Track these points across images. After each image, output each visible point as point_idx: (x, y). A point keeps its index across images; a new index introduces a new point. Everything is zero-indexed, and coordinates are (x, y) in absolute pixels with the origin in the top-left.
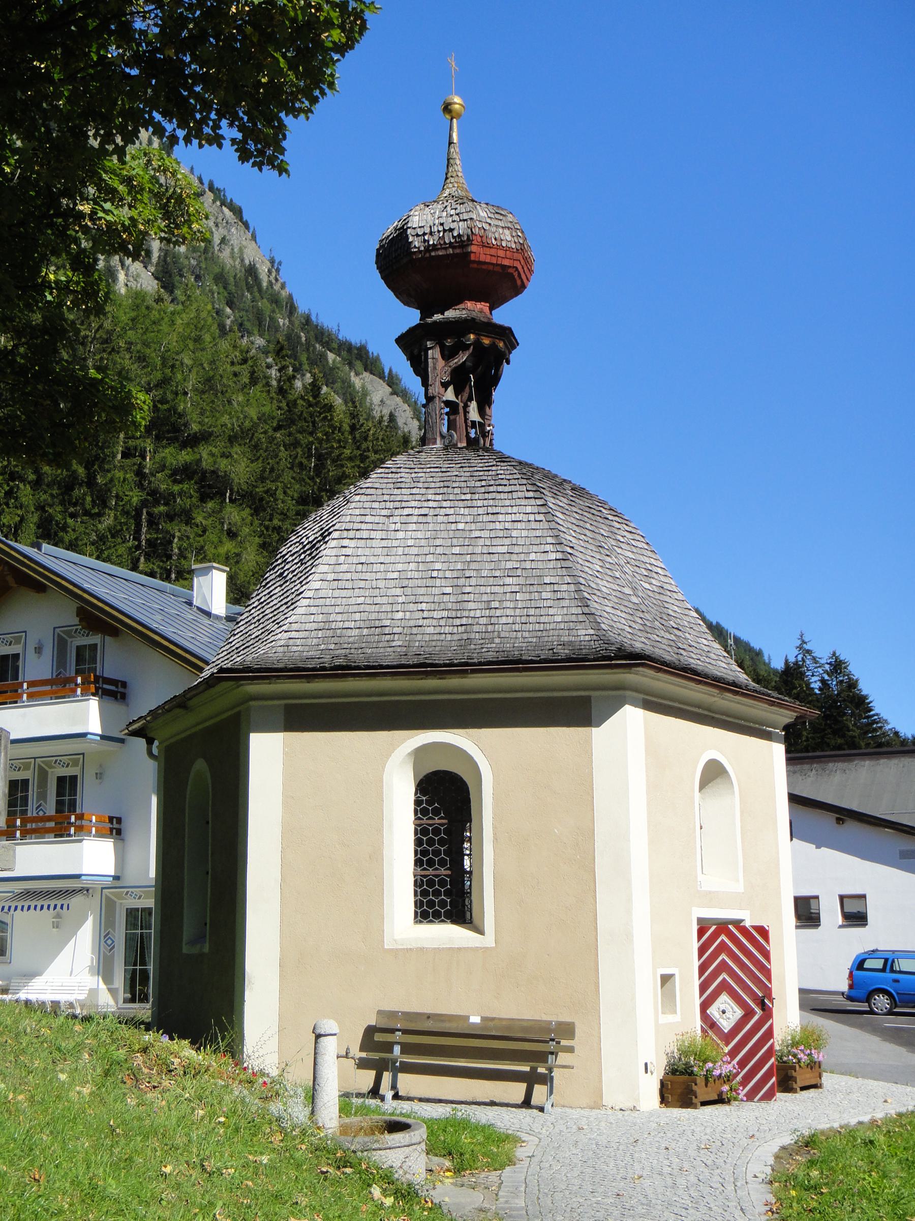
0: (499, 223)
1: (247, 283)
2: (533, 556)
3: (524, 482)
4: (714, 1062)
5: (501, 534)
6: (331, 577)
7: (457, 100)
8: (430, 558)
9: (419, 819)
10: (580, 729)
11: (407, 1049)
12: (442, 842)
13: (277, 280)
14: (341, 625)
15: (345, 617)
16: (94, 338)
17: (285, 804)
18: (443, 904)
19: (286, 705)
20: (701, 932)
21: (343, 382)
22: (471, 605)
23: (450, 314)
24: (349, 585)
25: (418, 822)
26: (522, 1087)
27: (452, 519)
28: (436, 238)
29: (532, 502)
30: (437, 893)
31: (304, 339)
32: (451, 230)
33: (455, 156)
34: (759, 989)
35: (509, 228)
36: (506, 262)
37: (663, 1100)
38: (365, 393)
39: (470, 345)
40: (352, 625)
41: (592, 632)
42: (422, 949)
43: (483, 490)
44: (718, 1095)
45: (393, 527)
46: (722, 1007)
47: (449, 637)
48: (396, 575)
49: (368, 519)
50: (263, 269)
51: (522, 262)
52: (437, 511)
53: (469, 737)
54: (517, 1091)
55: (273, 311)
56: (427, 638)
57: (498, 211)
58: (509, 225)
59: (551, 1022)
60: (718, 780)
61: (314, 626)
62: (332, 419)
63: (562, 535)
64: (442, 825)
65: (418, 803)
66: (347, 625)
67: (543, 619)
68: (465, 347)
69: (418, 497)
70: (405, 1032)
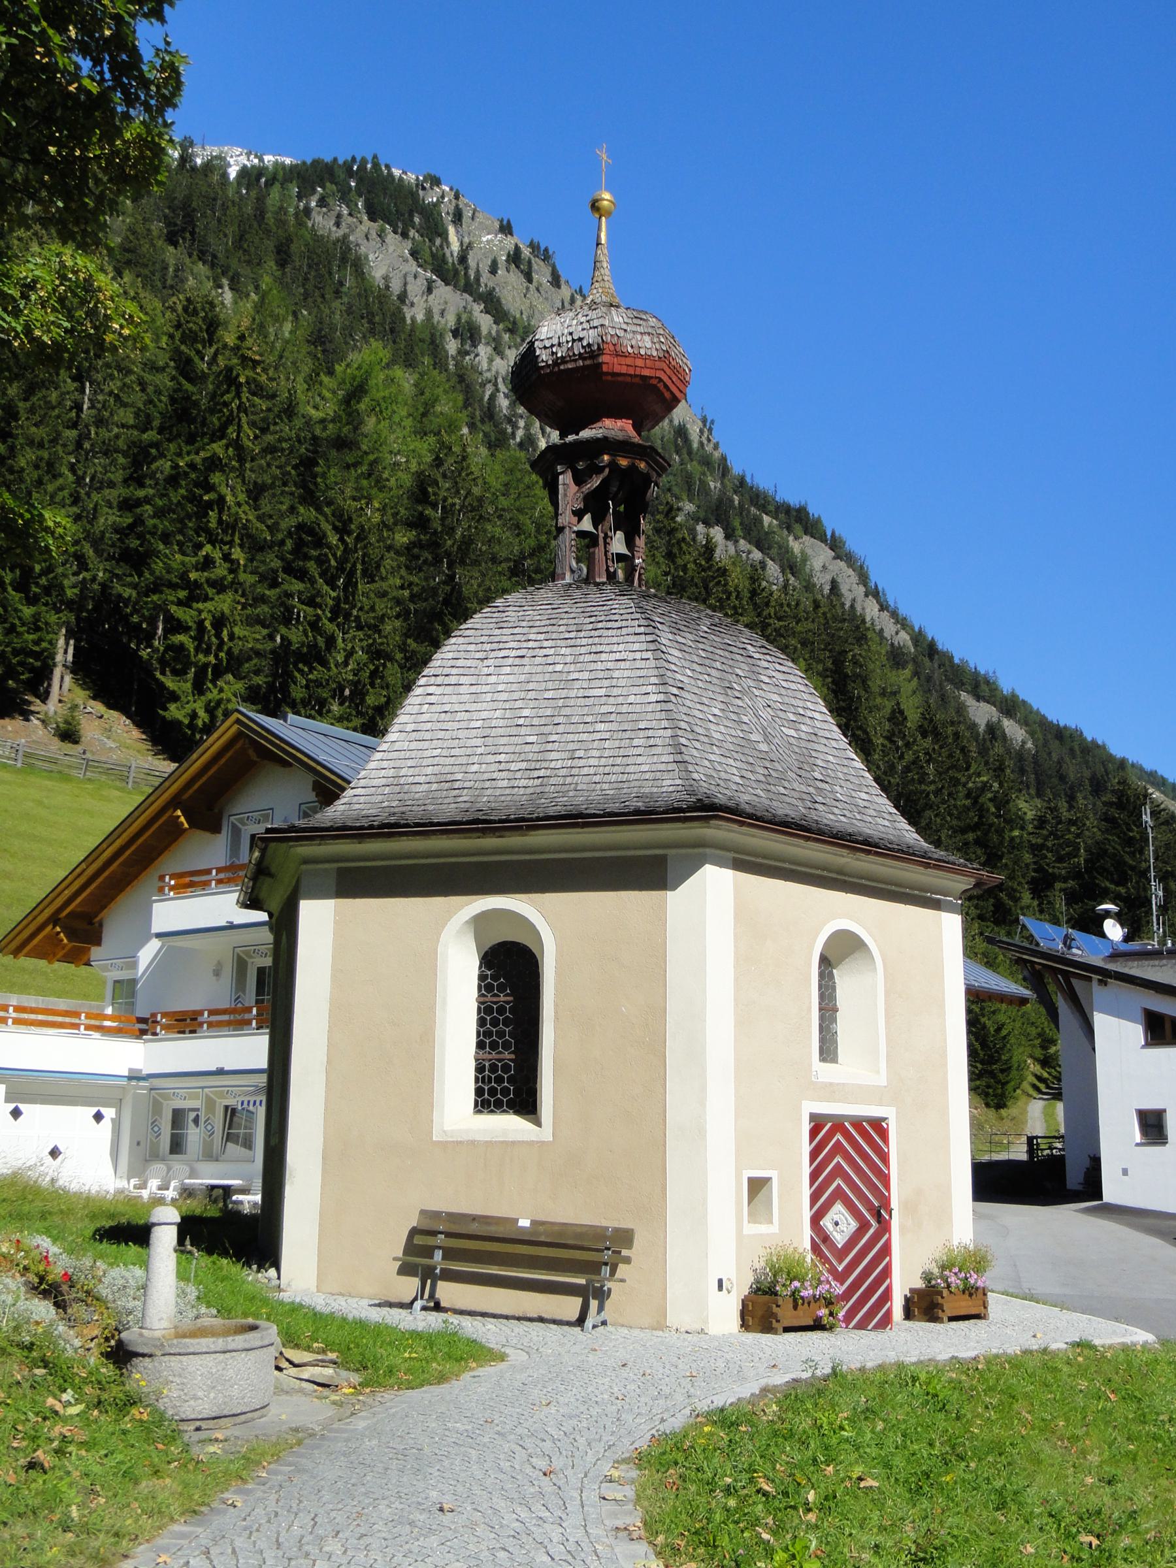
0: (638, 329)
1: (676, 445)
2: (631, 699)
3: (638, 616)
4: (803, 1282)
5: (601, 675)
6: (410, 728)
7: (606, 196)
8: (519, 704)
9: (483, 995)
10: (654, 893)
11: (449, 1254)
12: (506, 1022)
13: (709, 440)
14: (411, 780)
15: (416, 771)
16: (463, 506)
17: (334, 978)
18: (505, 1092)
19: (339, 869)
20: (814, 1133)
21: (780, 547)
22: (553, 755)
23: (586, 434)
24: (428, 736)
25: (482, 999)
26: (577, 1302)
27: (550, 660)
28: (564, 349)
29: (642, 638)
30: (499, 1080)
31: (736, 502)
32: (580, 339)
33: (602, 258)
34: (875, 1197)
35: (649, 334)
36: (646, 373)
37: (745, 1326)
38: (805, 558)
39: (603, 468)
40: (422, 779)
41: (679, 782)
42: (473, 1143)
43: (591, 626)
44: (815, 1321)
45: (486, 671)
46: (836, 1218)
47: (522, 791)
48: (479, 724)
49: (459, 663)
50: (694, 430)
51: (668, 371)
52: (536, 652)
53: (532, 904)
54: (570, 1306)
55: (704, 474)
56: (498, 792)
57: (638, 316)
58: (650, 330)
59: (607, 1228)
60: (857, 955)
61: (384, 781)
62: (726, 584)
63: (669, 674)
64: (508, 1002)
65: (482, 977)
66: (417, 779)
67: (628, 769)
68: (600, 470)
69: (518, 637)
70: (449, 1235)
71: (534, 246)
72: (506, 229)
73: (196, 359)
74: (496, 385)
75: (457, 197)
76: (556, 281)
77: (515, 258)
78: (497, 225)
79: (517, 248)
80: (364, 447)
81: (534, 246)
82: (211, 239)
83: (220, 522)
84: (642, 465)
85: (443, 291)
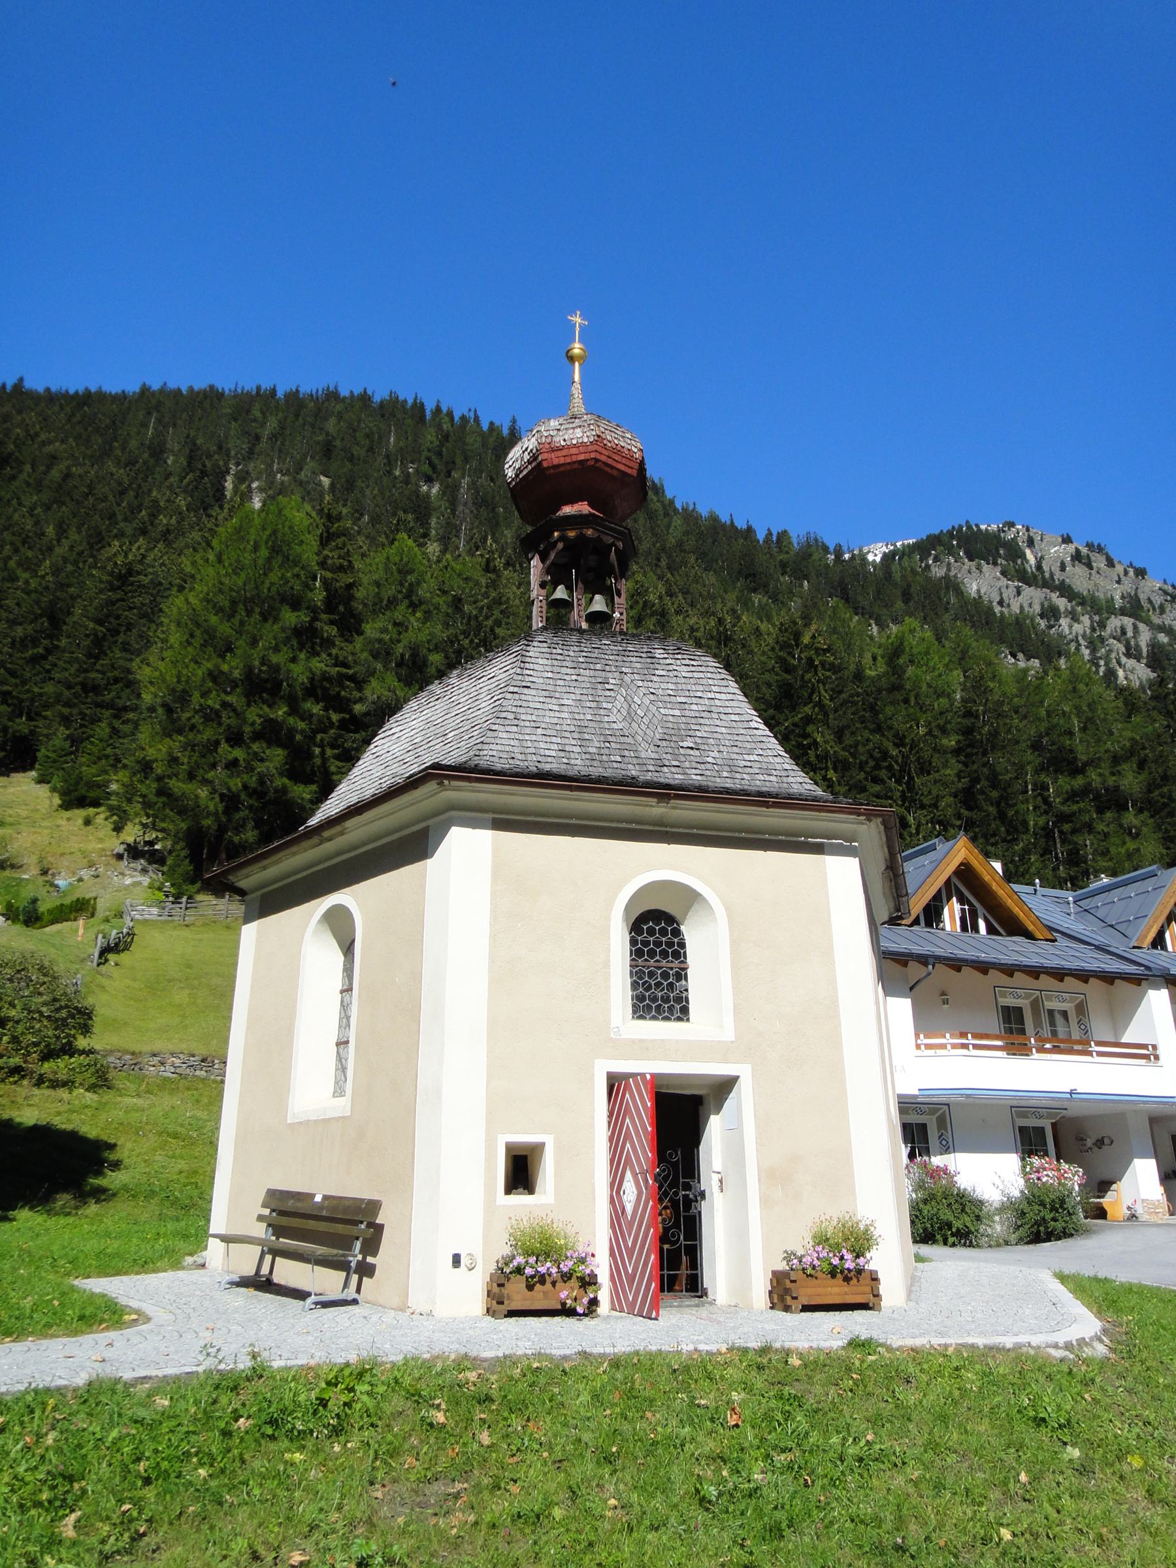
36: (582, 457)
54: (328, 1281)
60: (695, 907)
71: (1089, 546)
72: (1067, 540)
73: (789, 658)
74: (1077, 641)
75: (1028, 530)
76: (1111, 563)
77: (1077, 557)
78: (1060, 540)
79: (1077, 550)
80: (908, 687)
81: (1089, 546)
82: (860, 598)
83: (817, 756)
84: (590, 532)
85: (1028, 591)
